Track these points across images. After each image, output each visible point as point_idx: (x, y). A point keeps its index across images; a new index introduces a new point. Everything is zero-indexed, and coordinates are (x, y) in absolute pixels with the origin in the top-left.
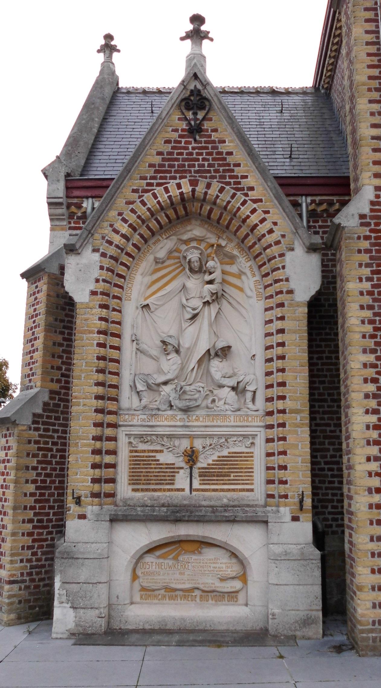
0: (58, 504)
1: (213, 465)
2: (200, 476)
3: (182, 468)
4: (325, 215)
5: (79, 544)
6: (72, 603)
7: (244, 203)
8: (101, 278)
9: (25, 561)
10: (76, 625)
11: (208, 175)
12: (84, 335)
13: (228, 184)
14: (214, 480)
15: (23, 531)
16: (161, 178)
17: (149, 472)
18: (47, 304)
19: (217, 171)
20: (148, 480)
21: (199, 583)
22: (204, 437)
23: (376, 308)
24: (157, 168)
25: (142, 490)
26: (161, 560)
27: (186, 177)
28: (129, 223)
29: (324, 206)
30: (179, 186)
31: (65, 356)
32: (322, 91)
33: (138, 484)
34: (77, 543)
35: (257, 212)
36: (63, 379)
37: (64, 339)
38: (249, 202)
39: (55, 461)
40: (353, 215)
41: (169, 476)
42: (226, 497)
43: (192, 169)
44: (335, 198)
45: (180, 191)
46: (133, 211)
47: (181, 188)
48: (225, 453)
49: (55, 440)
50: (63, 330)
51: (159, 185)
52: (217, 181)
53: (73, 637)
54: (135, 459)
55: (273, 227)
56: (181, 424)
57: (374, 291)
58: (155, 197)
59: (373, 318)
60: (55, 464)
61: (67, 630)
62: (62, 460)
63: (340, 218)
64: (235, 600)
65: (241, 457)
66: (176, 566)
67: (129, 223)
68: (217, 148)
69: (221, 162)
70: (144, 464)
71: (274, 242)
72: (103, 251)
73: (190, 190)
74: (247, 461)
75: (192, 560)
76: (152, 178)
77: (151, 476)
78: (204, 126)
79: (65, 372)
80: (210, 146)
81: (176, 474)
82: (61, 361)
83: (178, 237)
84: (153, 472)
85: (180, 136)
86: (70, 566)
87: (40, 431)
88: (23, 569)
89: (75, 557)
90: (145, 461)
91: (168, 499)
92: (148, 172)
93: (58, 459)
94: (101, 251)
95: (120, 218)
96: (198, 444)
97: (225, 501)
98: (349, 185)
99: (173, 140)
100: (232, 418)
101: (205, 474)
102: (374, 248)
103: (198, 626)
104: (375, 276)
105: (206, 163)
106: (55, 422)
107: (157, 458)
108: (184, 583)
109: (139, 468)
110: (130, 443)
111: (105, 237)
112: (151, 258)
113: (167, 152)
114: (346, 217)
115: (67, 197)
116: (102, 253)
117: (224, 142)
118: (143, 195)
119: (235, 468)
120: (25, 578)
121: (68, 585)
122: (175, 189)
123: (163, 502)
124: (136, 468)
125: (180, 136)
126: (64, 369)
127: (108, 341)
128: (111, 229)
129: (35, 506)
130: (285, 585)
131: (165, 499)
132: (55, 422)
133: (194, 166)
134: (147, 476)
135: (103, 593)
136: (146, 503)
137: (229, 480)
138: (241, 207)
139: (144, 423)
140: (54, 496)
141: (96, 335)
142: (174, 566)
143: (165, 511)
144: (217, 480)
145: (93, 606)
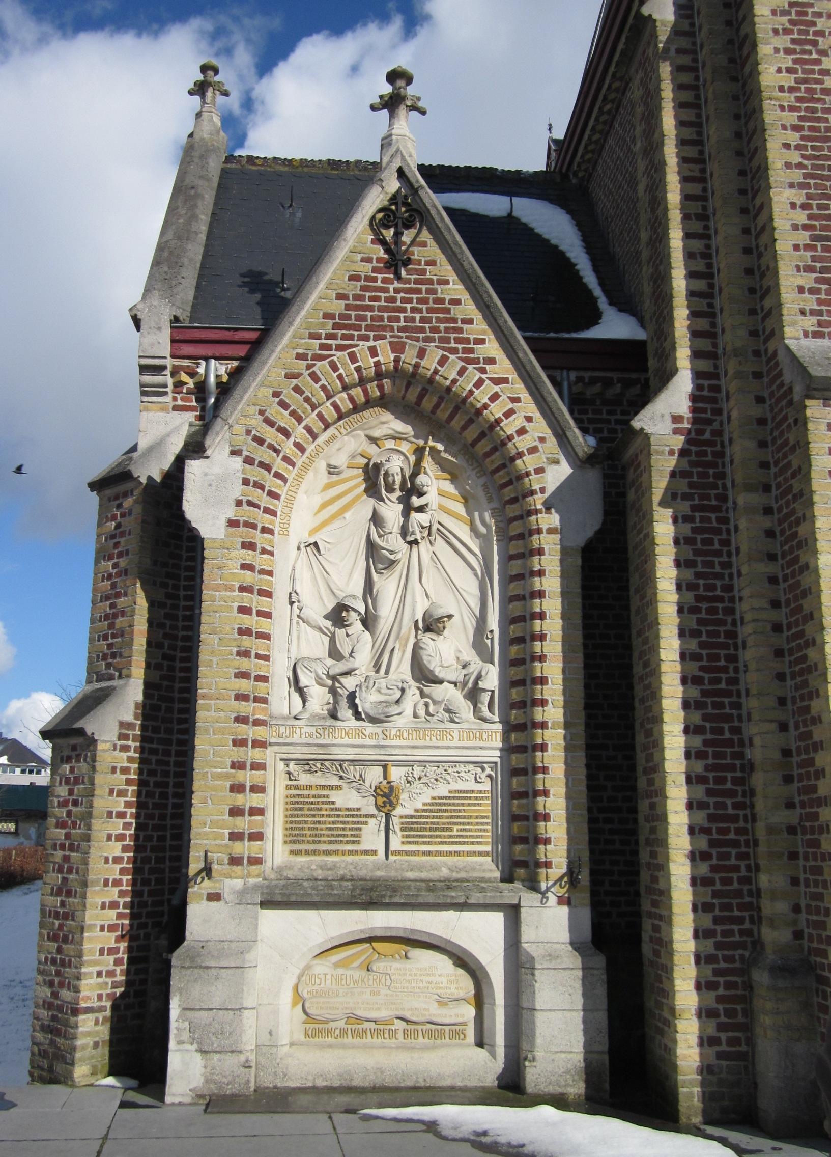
0: (156, 876)
1: (423, 811)
2: (402, 830)
3: (373, 816)
4: (598, 402)
5: (209, 943)
6: (198, 1043)
7: (479, 383)
8: (244, 499)
9: (104, 973)
10: (207, 1081)
11: (421, 335)
12: (217, 593)
13: (454, 351)
14: (425, 836)
15: (102, 923)
16: (344, 337)
17: (318, 822)
18: (142, 537)
19: (435, 330)
20: (316, 836)
21: (403, 1009)
22: (410, 764)
23: (700, 565)
24: (337, 321)
25: (307, 853)
26: (340, 971)
27: (384, 338)
28: (291, 409)
29: (597, 388)
30: (373, 352)
31: (168, 623)
32: (574, 181)
33: (299, 842)
34: (207, 941)
35: (501, 399)
36: (166, 663)
37: (168, 596)
38: (487, 382)
39: (153, 803)
40: (662, 416)
41: (351, 829)
42: (445, 864)
43: (395, 325)
44: (615, 375)
45: (376, 359)
46: (297, 389)
47: (377, 356)
48: (443, 790)
49: (153, 767)
50: (167, 580)
51: (340, 348)
52: (436, 347)
53: (201, 1102)
54: (294, 800)
55: (526, 424)
56: (372, 742)
57: (696, 538)
58: (334, 368)
59: (694, 581)
60: (153, 809)
61: (190, 1090)
62: (163, 801)
63: (642, 419)
64: (462, 1036)
65: (469, 798)
66: (366, 980)
67: (291, 409)
68: (434, 292)
69: (441, 315)
70: (309, 810)
71: (528, 450)
72: (248, 454)
73: (392, 358)
74: (479, 805)
75: (393, 971)
76: (329, 336)
77: (322, 829)
78: (413, 255)
79: (168, 652)
80: (424, 287)
81: (363, 826)
82: (161, 632)
83: (367, 432)
84: (325, 823)
85: (375, 270)
86: (196, 981)
87: (129, 751)
88: (101, 988)
89: (203, 965)
90: (312, 803)
91: (351, 867)
92: (323, 326)
93: (157, 800)
94: (245, 453)
95: (277, 400)
96: (397, 774)
97: (445, 872)
98: (646, 360)
99: (363, 275)
100: (455, 735)
101: (411, 826)
102: (695, 470)
103: (404, 1080)
104: (697, 514)
105: (418, 316)
106: (153, 735)
107: (331, 799)
108: (378, 1009)
109: (301, 816)
110: (289, 773)
111: (251, 431)
112: (322, 465)
113: (353, 295)
114: (652, 418)
115: (173, 356)
116: (247, 457)
117: (447, 282)
118: (315, 365)
119: (459, 817)
120: (103, 1004)
121: (193, 1012)
122: (367, 356)
123: (342, 872)
124: (296, 816)
125: (375, 270)
126: (166, 647)
127: (255, 604)
128: (261, 418)
129: (121, 880)
130: (550, 1010)
131: (345, 868)
132: (153, 735)
133: (397, 320)
134: (316, 829)
135: (250, 1027)
136: (315, 874)
137: (450, 836)
138: (474, 389)
139: (311, 741)
140: (150, 862)
141: (237, 593)
142: (363, 981)
143: (350, 887)
144: (431, 836)
145: (234, 1048)
